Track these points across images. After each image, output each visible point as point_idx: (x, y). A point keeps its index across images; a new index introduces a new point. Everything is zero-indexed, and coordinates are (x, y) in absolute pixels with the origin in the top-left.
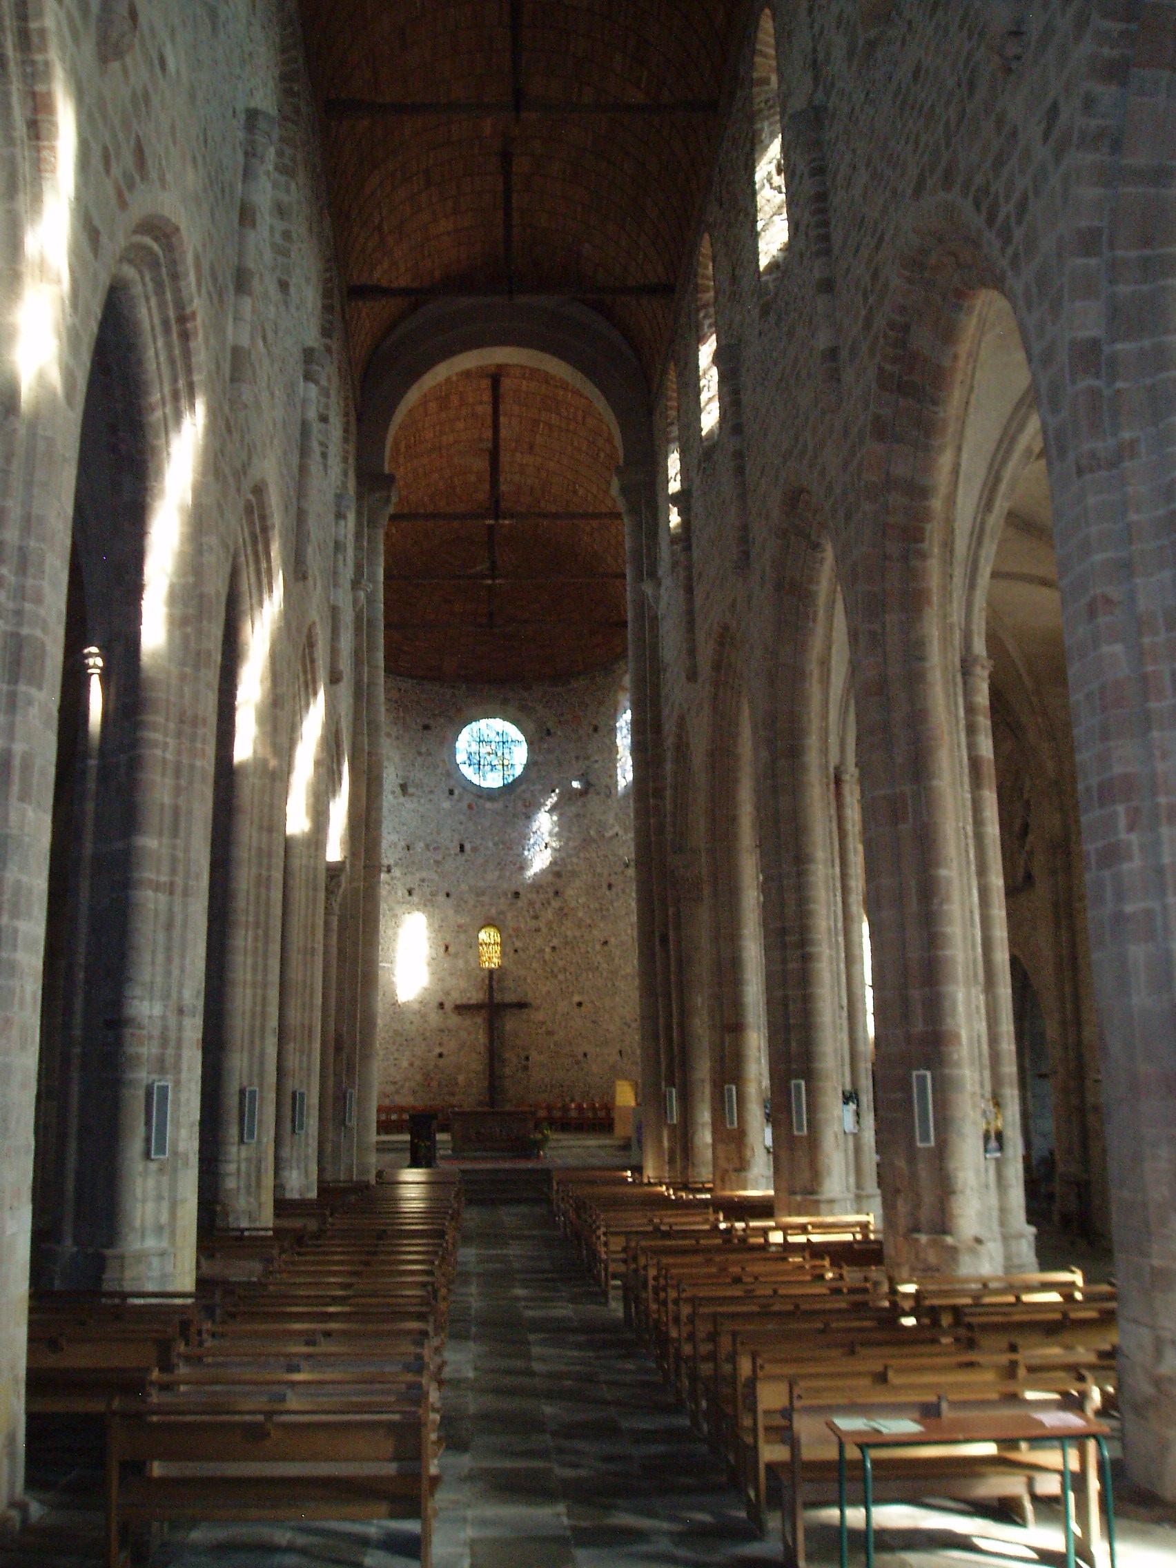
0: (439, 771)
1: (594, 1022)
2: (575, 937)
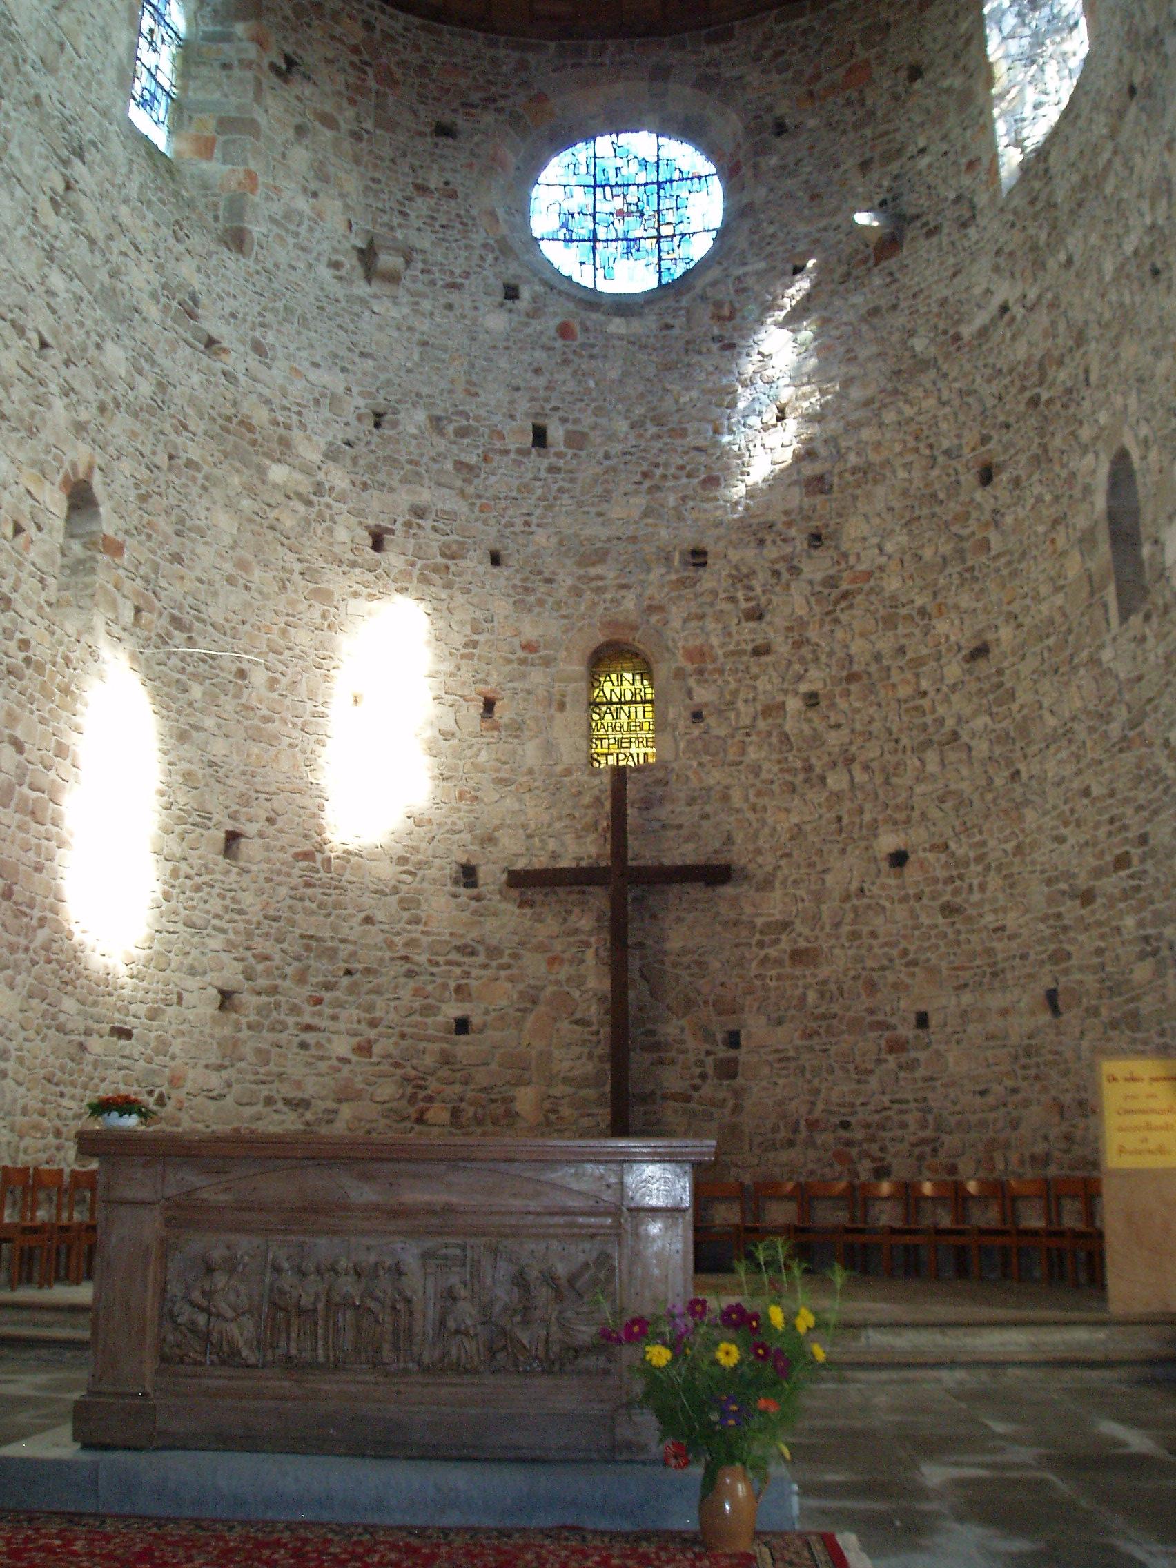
0: (478, 238)
1: (948, 910)
2: (878, 657)
